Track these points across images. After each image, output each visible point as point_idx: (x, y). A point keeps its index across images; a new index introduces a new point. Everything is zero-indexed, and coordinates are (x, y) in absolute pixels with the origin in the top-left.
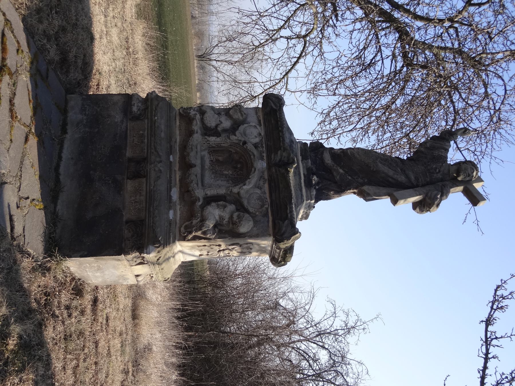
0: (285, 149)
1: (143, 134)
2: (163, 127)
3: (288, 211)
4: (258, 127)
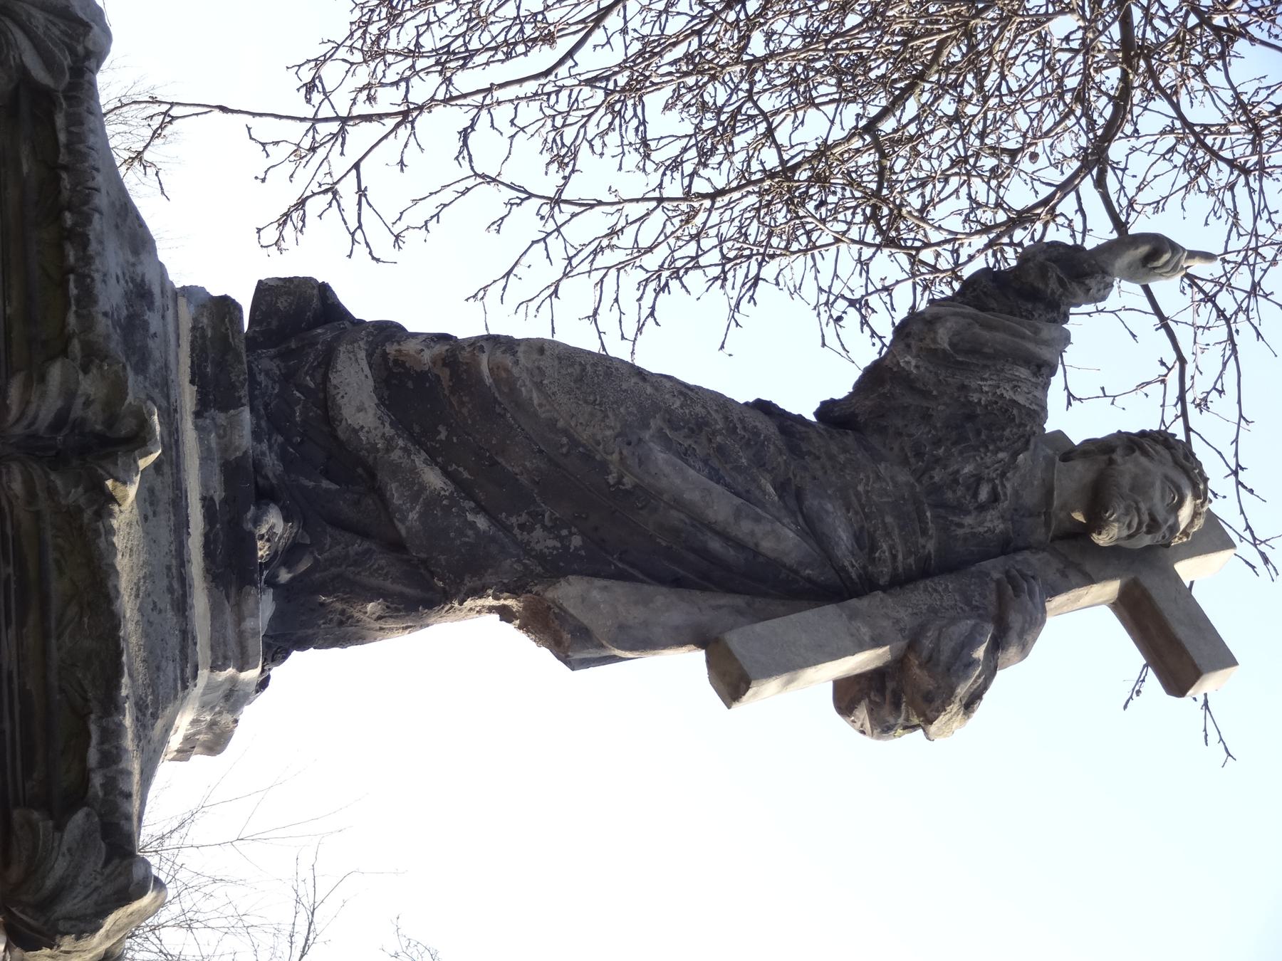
0: (93, 356)
3: (93, 756)
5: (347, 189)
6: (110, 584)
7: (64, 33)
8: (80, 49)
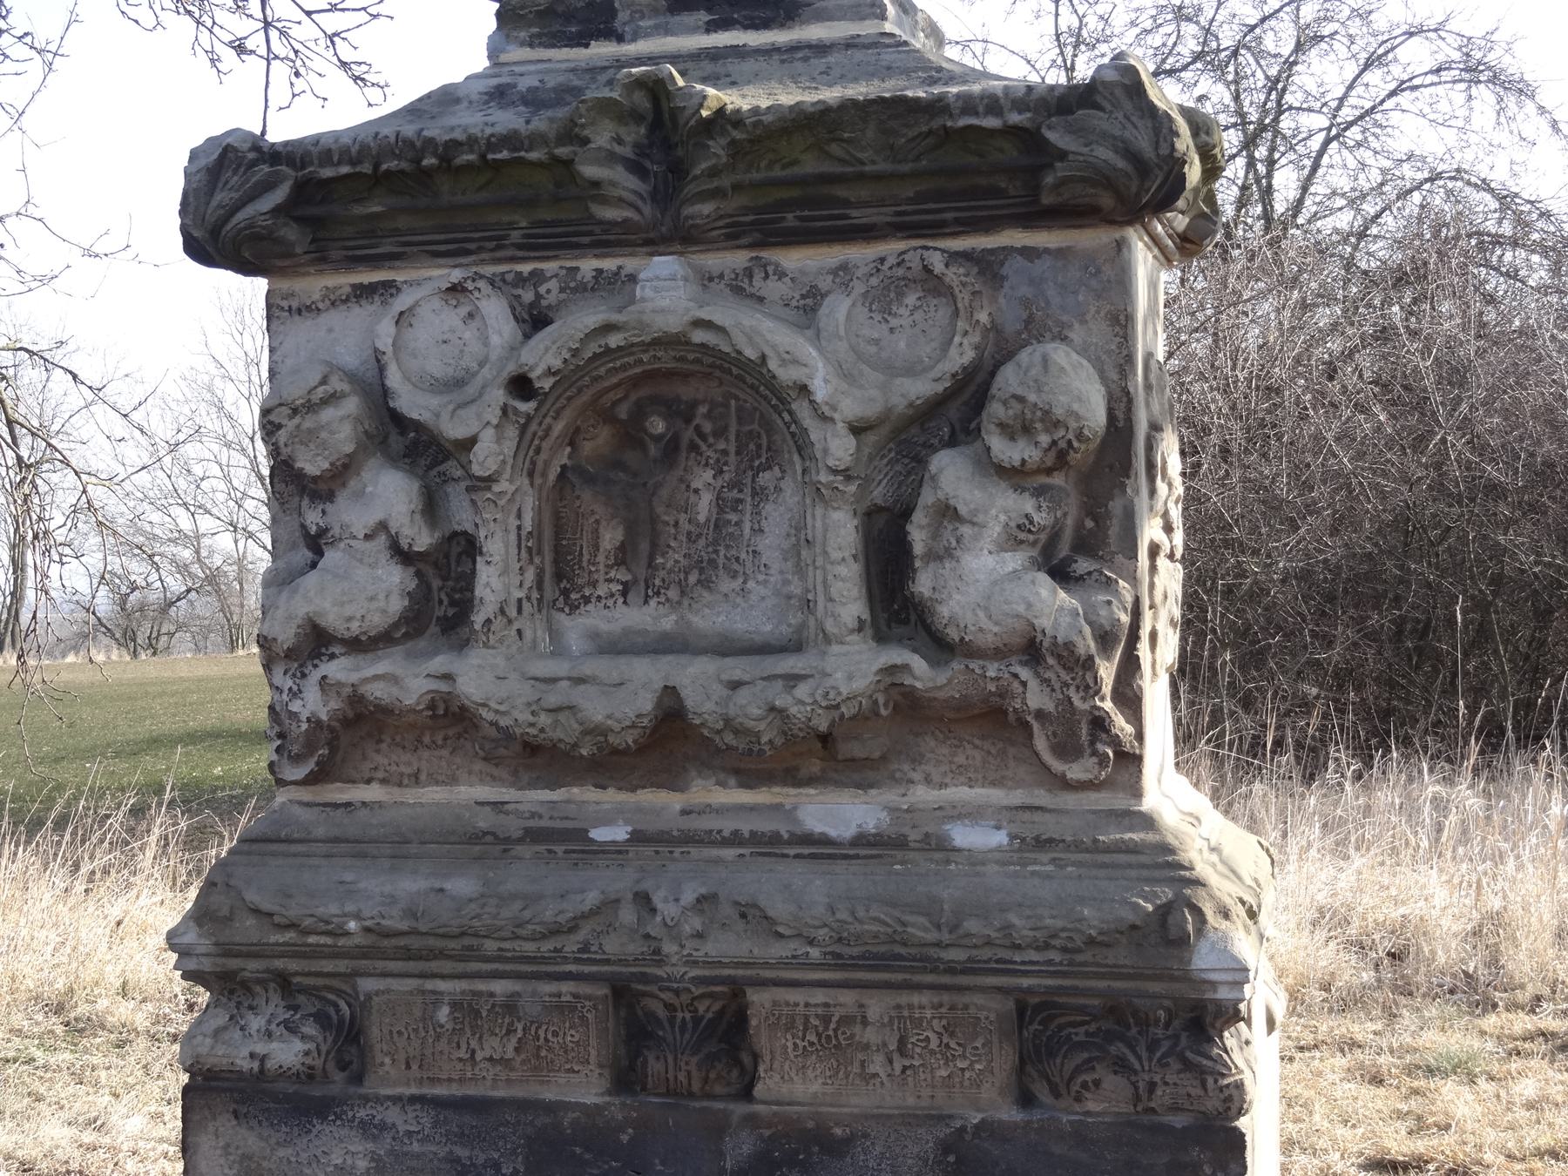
0: (571, 134)
1: (455, 1006)
2: (410, 885)
3: (991, 122)
4: (402, 302)
5: (332, 22)
6: (812, 109)
7: (235, 172)
8: (251, 156)
